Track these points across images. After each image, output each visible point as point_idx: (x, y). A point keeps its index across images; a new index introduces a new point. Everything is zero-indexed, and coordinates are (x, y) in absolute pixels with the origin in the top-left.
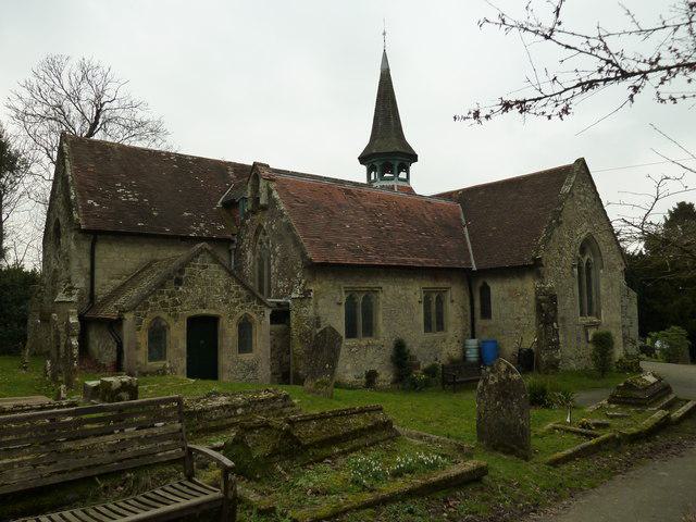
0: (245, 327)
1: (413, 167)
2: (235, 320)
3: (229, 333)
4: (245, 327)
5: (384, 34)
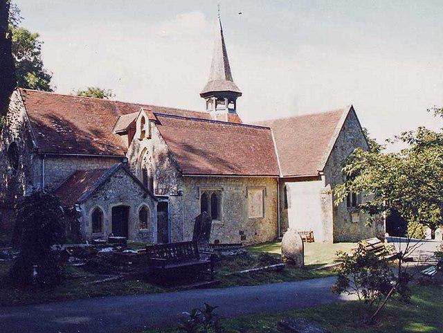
0: (143, 214)
1: (239, 100)
2: (138, 210)
3: (134, 214)
4: (143, 214)
5: (219, 6)
